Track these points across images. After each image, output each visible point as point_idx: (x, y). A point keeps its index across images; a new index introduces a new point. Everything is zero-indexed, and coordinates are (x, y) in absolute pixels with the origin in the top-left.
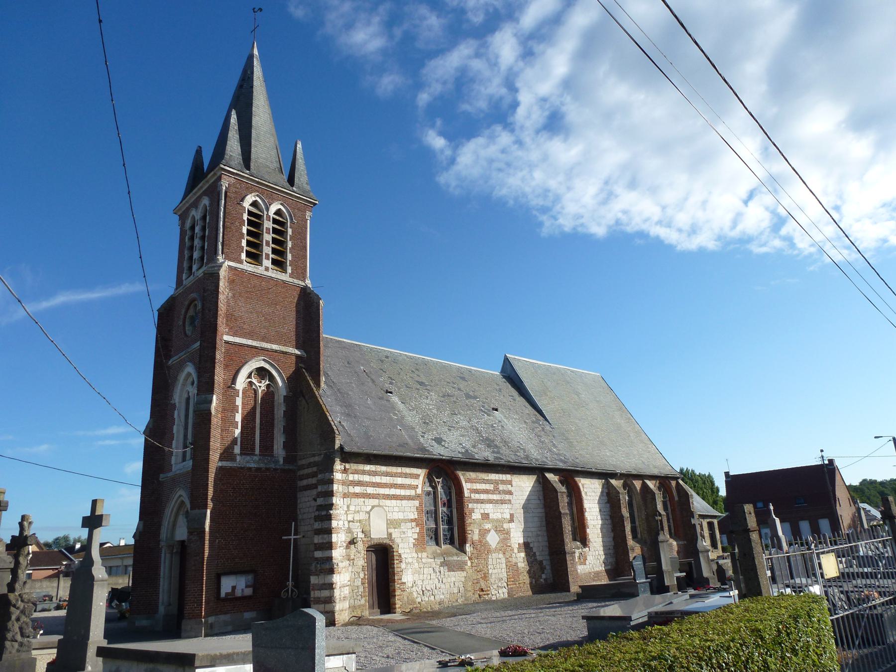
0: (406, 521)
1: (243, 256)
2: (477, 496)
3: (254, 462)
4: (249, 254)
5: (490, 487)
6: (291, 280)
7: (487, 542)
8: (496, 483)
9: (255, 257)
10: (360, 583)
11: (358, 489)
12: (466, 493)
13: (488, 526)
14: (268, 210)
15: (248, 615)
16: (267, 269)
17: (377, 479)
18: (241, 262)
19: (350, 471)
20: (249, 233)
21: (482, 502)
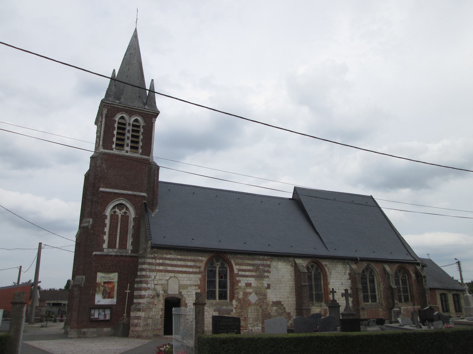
0: (191, 285)
1: (114, 146)
2: (243, 273)
3: (114, 252)
4: (117, 145)
5: (251, 268)
6: (141, 156)
7: (249, 300)
8: (258, 266)
9: (120, 146)
10: (159, 317)
11: (161, 268)
12: (236, 271)
13: (249, 290)
14: (130, 120)
15: (106, 330)
16: (127, 152)
17: (175, 262)
18: (112, 149)
19: (157, 258)
20: (118, 133)
21: (247, 276)
